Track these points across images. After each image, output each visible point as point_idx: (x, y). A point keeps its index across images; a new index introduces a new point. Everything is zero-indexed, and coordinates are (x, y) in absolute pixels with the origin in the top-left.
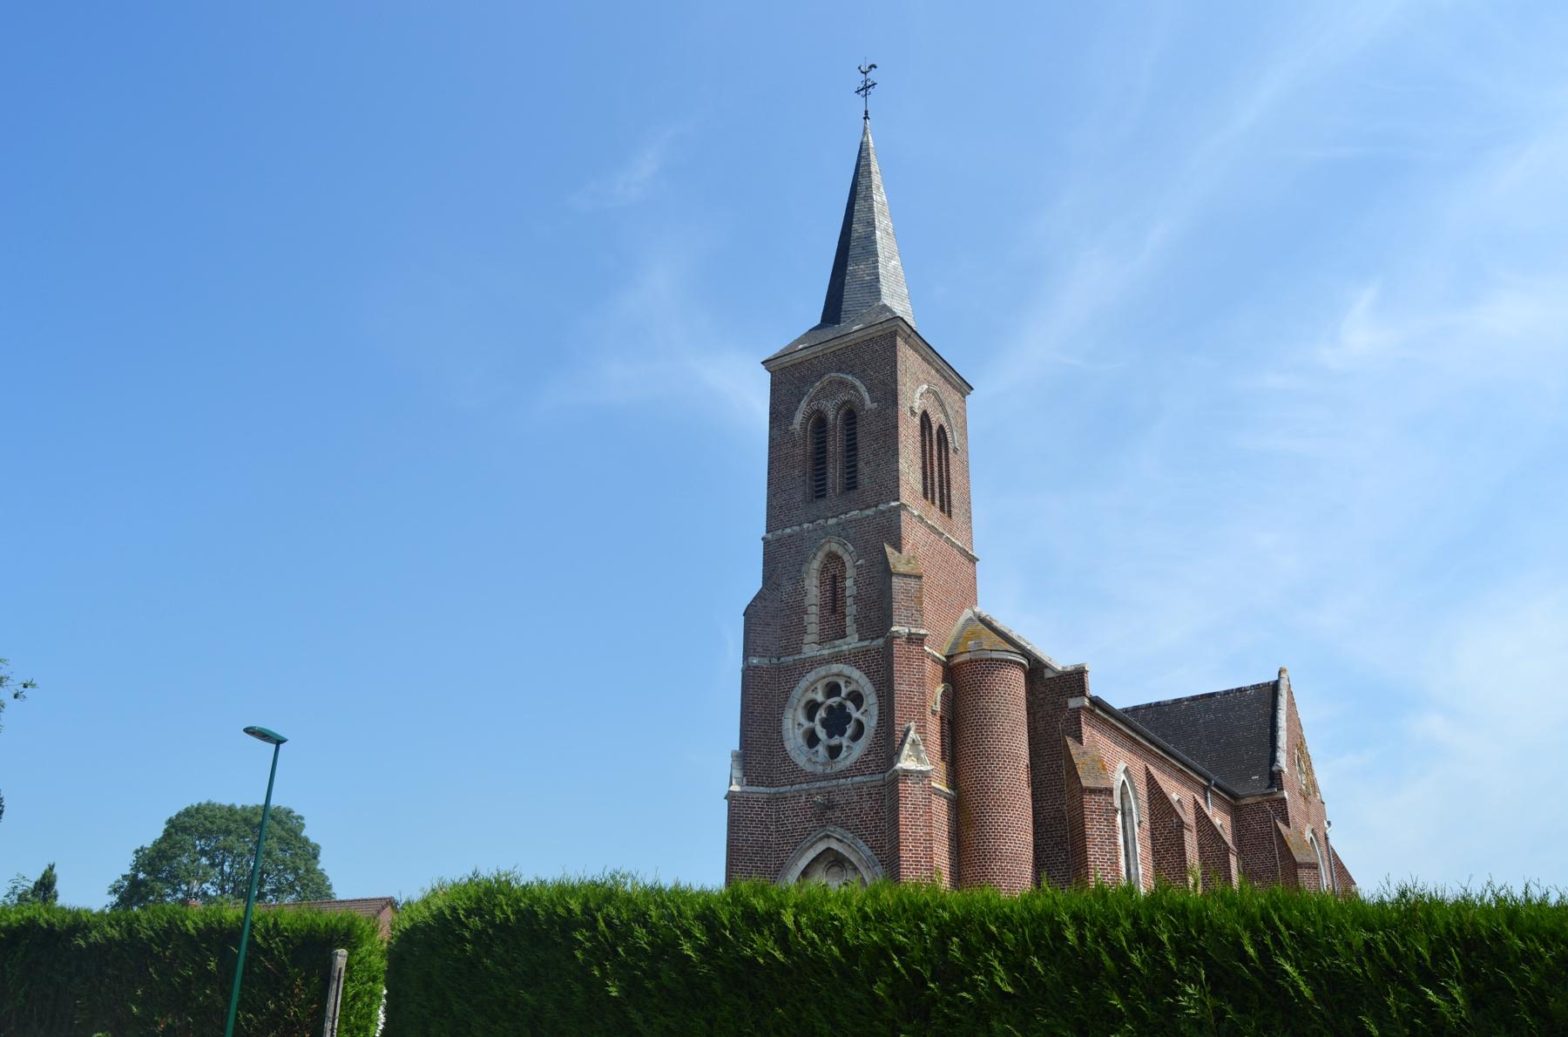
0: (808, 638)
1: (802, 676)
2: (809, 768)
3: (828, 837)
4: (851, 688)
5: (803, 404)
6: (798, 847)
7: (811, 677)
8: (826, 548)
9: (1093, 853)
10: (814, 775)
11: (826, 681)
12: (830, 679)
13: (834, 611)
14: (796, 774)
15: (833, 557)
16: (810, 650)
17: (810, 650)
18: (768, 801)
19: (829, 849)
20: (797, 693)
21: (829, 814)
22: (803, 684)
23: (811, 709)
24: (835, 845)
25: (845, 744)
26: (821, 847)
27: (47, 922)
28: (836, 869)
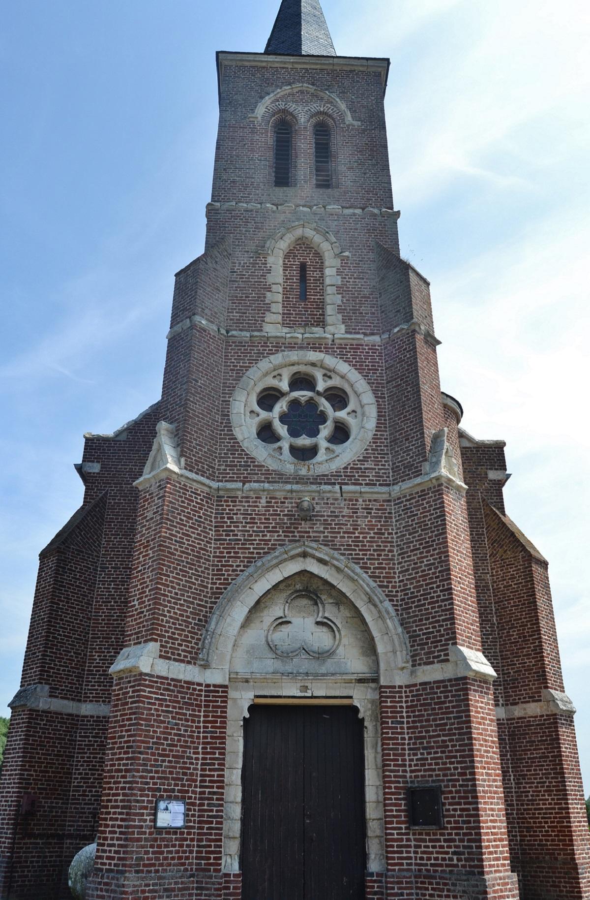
0: (269, 317)
1: (261, 355)
2: (272, 465)
3: (304, 555)
4: (330, 383)
5: (268, 100)
6: (254, 558)
7: (277, 359)
8: (299, 232)
9: (542, 623)
10: (280, 475)
11: (295, 369)
12: (302, 368)
13: (303, 296)
14: (248, 468)
15: (302, 244)
16: (273, 328)
17: (273, 328)
18: (208, 497)
19: (304, 572)
20: (254, 373)
21: (305, 526)
22: (264, 365)
23: (268, 398)
24: (314, 568)
25: (323, 444)
26: (292, 568)
27: (339, 611)
28: (305, 602)
